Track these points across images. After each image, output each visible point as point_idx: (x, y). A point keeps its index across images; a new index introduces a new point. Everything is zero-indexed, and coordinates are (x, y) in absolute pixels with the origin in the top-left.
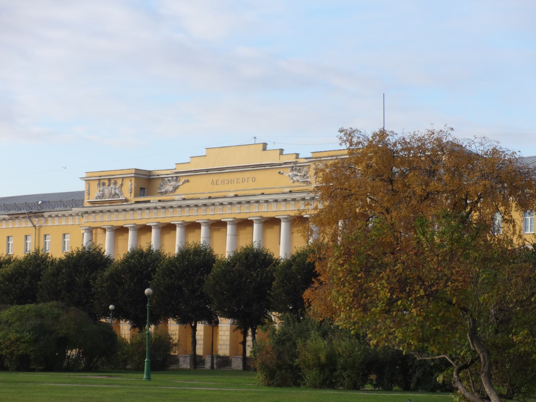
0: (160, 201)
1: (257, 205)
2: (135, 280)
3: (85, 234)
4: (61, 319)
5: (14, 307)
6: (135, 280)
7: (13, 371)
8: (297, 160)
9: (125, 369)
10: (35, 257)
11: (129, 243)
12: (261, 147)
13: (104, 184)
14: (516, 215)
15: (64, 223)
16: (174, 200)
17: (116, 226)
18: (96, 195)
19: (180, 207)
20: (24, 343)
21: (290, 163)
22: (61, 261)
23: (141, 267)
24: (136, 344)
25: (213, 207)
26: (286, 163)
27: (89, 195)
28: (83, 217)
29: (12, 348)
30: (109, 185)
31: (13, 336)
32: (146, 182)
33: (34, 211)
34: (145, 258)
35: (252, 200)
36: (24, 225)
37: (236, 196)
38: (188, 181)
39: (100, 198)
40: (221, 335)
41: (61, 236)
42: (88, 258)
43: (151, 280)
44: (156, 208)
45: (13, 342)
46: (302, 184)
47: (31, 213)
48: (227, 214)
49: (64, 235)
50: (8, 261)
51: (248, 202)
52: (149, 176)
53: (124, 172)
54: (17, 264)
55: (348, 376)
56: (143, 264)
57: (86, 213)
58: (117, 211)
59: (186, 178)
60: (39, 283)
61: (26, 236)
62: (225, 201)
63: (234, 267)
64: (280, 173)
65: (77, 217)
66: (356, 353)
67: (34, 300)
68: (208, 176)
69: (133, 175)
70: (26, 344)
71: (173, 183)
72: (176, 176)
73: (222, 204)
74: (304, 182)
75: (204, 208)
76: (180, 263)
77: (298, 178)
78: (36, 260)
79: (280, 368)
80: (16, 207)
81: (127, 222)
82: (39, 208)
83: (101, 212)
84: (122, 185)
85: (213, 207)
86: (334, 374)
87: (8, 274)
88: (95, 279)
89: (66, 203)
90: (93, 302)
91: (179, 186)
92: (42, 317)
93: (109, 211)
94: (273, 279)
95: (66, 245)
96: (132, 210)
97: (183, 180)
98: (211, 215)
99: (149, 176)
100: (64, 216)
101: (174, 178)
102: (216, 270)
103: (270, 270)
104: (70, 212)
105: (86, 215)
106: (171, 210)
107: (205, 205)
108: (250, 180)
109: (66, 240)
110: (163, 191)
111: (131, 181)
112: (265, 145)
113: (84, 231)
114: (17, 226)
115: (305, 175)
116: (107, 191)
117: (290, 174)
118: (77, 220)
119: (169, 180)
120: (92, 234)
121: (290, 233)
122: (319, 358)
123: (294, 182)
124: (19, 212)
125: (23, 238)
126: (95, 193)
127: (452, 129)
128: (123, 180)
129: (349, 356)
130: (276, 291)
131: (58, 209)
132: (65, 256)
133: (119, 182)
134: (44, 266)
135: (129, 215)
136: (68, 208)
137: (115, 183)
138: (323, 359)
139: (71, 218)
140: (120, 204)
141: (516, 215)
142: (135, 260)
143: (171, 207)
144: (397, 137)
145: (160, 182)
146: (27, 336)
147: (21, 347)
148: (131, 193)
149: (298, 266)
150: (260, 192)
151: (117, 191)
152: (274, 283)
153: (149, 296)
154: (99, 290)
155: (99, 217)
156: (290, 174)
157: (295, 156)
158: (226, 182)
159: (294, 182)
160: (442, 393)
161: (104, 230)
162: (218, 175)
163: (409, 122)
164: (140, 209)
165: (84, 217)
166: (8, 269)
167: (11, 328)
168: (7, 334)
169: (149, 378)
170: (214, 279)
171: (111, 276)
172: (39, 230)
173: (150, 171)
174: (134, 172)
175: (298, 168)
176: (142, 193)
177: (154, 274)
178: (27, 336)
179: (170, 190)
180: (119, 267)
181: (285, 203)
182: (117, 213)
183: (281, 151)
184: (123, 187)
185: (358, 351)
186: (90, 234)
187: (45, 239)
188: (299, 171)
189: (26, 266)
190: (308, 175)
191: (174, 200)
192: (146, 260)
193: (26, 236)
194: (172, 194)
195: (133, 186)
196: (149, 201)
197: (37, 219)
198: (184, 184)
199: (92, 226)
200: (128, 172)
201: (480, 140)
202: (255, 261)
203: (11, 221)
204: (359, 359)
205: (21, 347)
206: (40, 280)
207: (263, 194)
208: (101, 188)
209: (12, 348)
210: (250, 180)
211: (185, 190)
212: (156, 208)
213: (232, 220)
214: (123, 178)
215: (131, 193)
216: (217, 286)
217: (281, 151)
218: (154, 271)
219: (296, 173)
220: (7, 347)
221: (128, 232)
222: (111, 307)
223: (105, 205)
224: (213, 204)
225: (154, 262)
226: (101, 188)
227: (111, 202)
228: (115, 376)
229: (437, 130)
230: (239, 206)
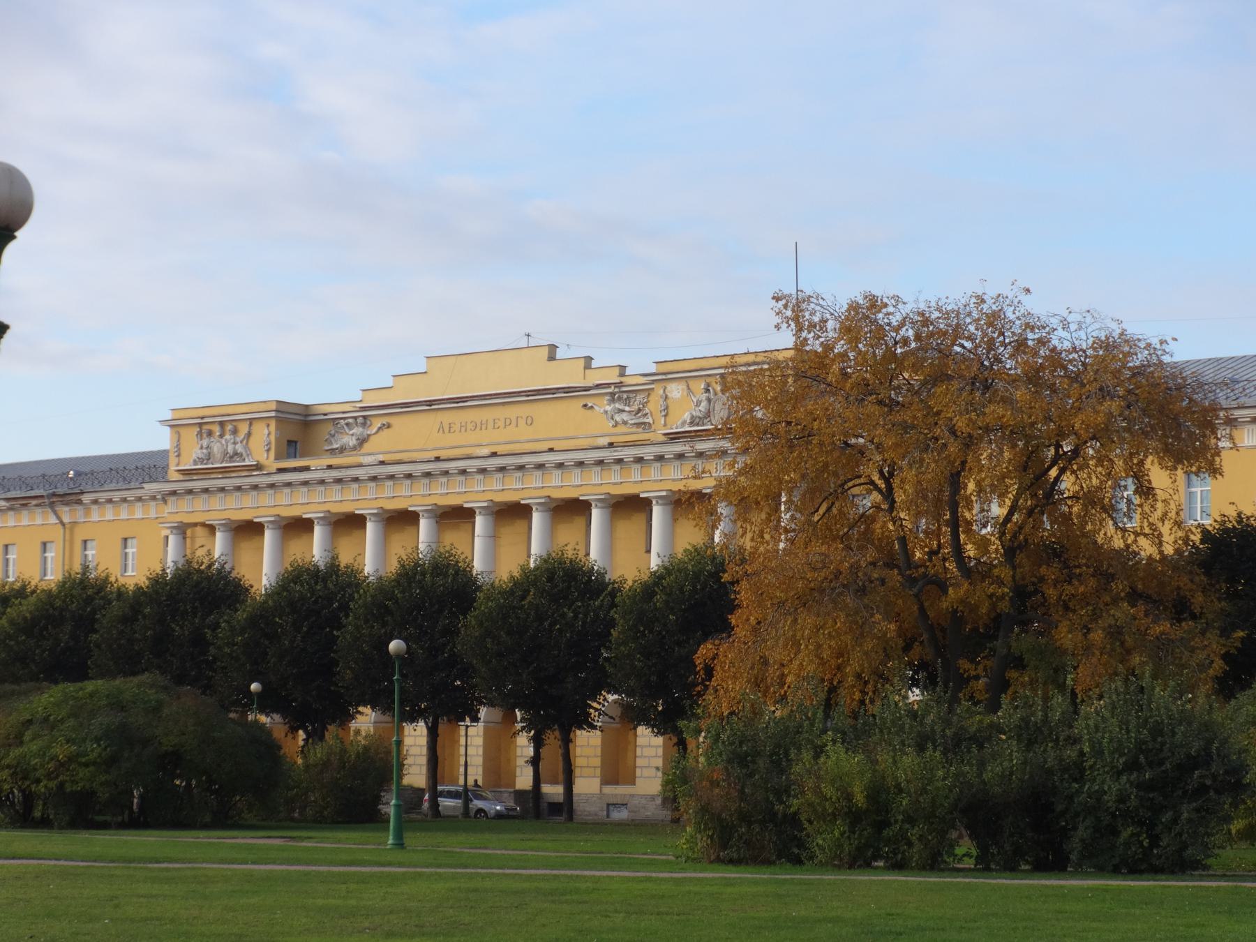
0: (330, 467)
1: (539, 473)
2: (305, 629)
3: (172, 539)
4: (166, 711)
5: (61, 686)
6: (305, 629)
7: (61, 828)
8: (623, 379)
9: (292, 819)
10: (82, 581)
11: (538, 540)
12: (545, 352)
13: (210, 434)
14: (1158, 477)
15: (124, 515)
16: (360, 465)
18: (194, 456)
19: (374, 478)
20: (86, 765)
21: (608, 385)
22: (139, 588)
23: (316, 602)
24: (316, 766)
25: (444, 480)
26: (598, 386)
27: (178, 456)
28: (165, 501)
29: (61, 778)
30: (221, 436)
31: (61, 751)
32: (299, 428)
33: (60, 491)
34: (325, 580)
35: (529, 463)
36: (39, 521)
37: (494, 454)
38: (389, 426)
40: (642, 747)
41: (120, 544)
42: (198, 583)
43: (338, 629)
44: (322, 482)
45: (62, 765)
46: (634, 430)
47: (54, 495)
48: (477, 493)
49: (126, 539)
50: (21, 592)
51: (521, 468)
52: (307, 415)
54: (43, 597)
55: (921, 838)
56: (319, 597)
57: (174, 493)
58: (239, 488)
59: (385, 420)
60: (95, 637)
61: (44, 544)
62: (648, 452)
63: (523, 598)
64: (585, 406)
65: (153, 503)
66: (940, 784)
67: (79, 673)
68: (432, 416)
69: (273, 414)
70: (92, 768)
71: (357, 430)
72: (364, 415)
73: (463, 472)
74: (638, 425)
75: (426, 481)
76: (403, 592)
77: (625, 416)
78: (84, 588)
79: (745, 818)
80: (23, 482)
81: (308, 508)
82: (71, 485)
83: (206, 491)
84: (249, 435)
86: (885, 833)
87: (25, 619)
88: (216, 626)
89: (128, 475)
90: (232, 678)
91: (369, 436)
92: (123, 709)
93: (222, 490)
94: (612, 623)
95: (130, 562)
96: (272, 486)
97: (377, 423)
98: (441, 495)
99: (307, 415)
100: (124, 500)
101: (360, 420)
102: (482, 605)
103: (601, 606)
104: (139, 493)
105: (171, 499)
106: (355, 486)
107: (428, 475)
108: (522, 422)
109: (130, 551)
110: (335, 446)
112: (553, 348)
113: (167, 532)
114: (25, 522)
115: (639, 410)
116: (216, 448)
117: (608, 408)
118: (153, 510)
119: (347, 424)
120: (185, 538)
121: (494, 537)
122: (849, 797)
123: (616, 424)
124: (28, 494)
125: (39, 548)
126: (192, 454)
127: (1028, 290)
128: (251, 424)
129: (924, 791)
130: (622, 648)
131: (112, 486)
132: (148, 579)
133: (244, 429)
134: (102, 602)
135: (267, 498)
136: (133, 485)
137: (235, 432)
138: (860, 799)
139: (140, 504)
141: (1158, 477)
142: (302, 585)
143: (356, 480)
144: (906, 309)
145: (330, 428)
146: (92, 751)
147: (81, 775)
148: (268, 450)
149: (669, 595)
150: (546, 446)
151: (239, 448)
152: (614, 633)
153: (399, 656)
154: (227, 650)
155: (200, 503)
156: (608, 408)
157: (617, 371)
158: (470, 426)
159: (616, 424)
160: (1132, 877)
161: (211, 529)
162: (454, 412)
163: (926, 277)
164: (289, 484)
165: (169, 502)
166: (25, 608)
167: (55, 732)
168: (49, 747)
169: (400, 844)
170: (481, 624)
171: (253, 621)
172: (72, 530)
173: (307, 406)
174: (274, 407)
175: (625, 396)
176: (292, 450)
177: (347, 616)
178: (94, 750)
180: (270, 602)
181: (599, 469)
182: (238, 494)
183: (589, 359)
184: (252, 439)
185: (944, 779)
187: (85, 549)
188: (628, 402)
189: (64, 601)
191: (360, 465)
192: (325, 586)
193: (44, 544)
195: (273, 438)
196: (306, 469)
197: (66, 509)
198: (381, 433)
199: (186, 521)
200: (263, 407)
201: (1079, 318)
202: (565, 582)
203: (11, 513)
204: (947, 797)
205: (81, 775)
206: (96, 631)
207: (551, 450)
208: (205, 443)
209: (61, 778)
210: (522, 422)
211: (382, 444)
212: (322, 482)
213: (485, 504)
214: (251, 421)
215: (268, 450)
216: (488, 640)
217: (589, 359)
218: (345, 608)
219: (621, 407)
220: (49, 776)
221: (262, 533)
222: (255, 687)
224: (446, 473)
225: (343, 589)
226: (205, 443)
227: (225, 471)
228: (302, 839)
229: (991, 292)
230: (501, 475)
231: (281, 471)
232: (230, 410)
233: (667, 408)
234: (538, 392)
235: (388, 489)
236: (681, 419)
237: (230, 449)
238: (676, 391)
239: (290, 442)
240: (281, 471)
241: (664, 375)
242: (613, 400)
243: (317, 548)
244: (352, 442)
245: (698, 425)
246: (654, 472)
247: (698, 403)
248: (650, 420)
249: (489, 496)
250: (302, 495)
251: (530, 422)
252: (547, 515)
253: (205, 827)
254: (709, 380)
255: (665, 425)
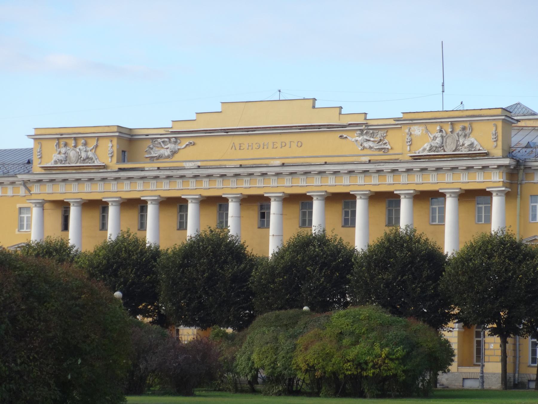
17: (245, 195)
21: (357, 125)
26: (350, 125)
30: (75, 146)
32: (129, 142)
35: (314, 171)
39: (61, 163)
52: (133, 135)
53: (101, 130)
59: (191, 141)
64: (341, 136)
69: (117, 134)
71: (171, 146)
72: (175, 135)
77: (371, 144)
81: (106, 195)
84: (97, 146)
85: (249, 179)
87: (9, 251)
91: (179, 149)
98: (246, 188)
107: (236, 175)
108: (294, 145)
111: (111, 141)
116: (72, 154)
126: (52, 156)
128: (98, 140)
137: (85, 144)
140: (74, 171)
148: (112, 157)
150: (323, 161)
151: (90, 154)
156: (359, 139)
158: (255, 146)
164: (129, 178)
173: (130, 129)
174: (115, 129)
179: (166, 154)
184: (98, 150)
186: (41, 209)
190: (386, 141)
194: (168, 160)
195: (115, 149)
196: (142, 170)
198: (188, 147)
210: (294, 145)
219: (368, 138)
223: (68, 171)
231: (121, 170)
232: (81, 131)
233: (411, 140)
234: (305, 127)
235: (205, 183)
236: (423, 148)
237: (83, 155)
238: (417, 130)
239: (124, 152)
240: (121, 170)
241: (408, 121)
242: (362, 134)
243: (319, 219)
244: (167, 153)
245: (434, 151)
246: (403, 179)
247: (435, 138)
248: (388, 147)
249: (282, 190)
250: (139, 186)
251: (300, 145)
252: (118, 208)
253: (397, 397)
254: (442, 124)
255: (410, 151)
